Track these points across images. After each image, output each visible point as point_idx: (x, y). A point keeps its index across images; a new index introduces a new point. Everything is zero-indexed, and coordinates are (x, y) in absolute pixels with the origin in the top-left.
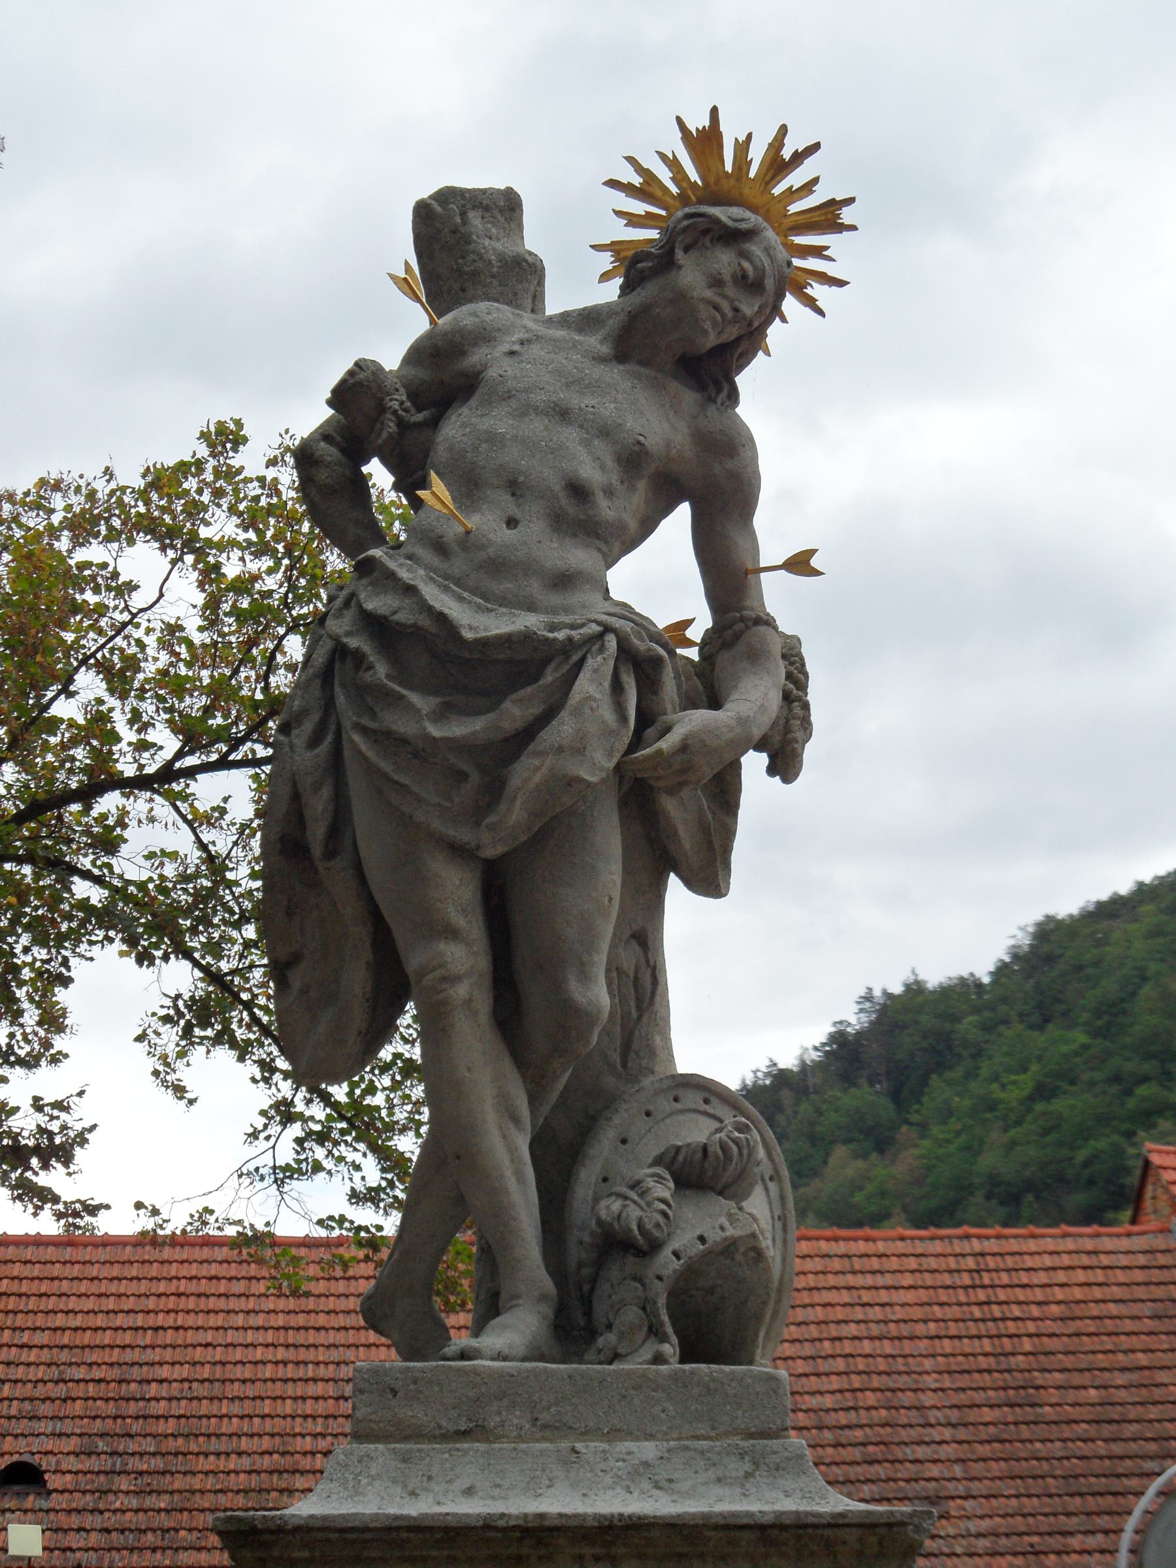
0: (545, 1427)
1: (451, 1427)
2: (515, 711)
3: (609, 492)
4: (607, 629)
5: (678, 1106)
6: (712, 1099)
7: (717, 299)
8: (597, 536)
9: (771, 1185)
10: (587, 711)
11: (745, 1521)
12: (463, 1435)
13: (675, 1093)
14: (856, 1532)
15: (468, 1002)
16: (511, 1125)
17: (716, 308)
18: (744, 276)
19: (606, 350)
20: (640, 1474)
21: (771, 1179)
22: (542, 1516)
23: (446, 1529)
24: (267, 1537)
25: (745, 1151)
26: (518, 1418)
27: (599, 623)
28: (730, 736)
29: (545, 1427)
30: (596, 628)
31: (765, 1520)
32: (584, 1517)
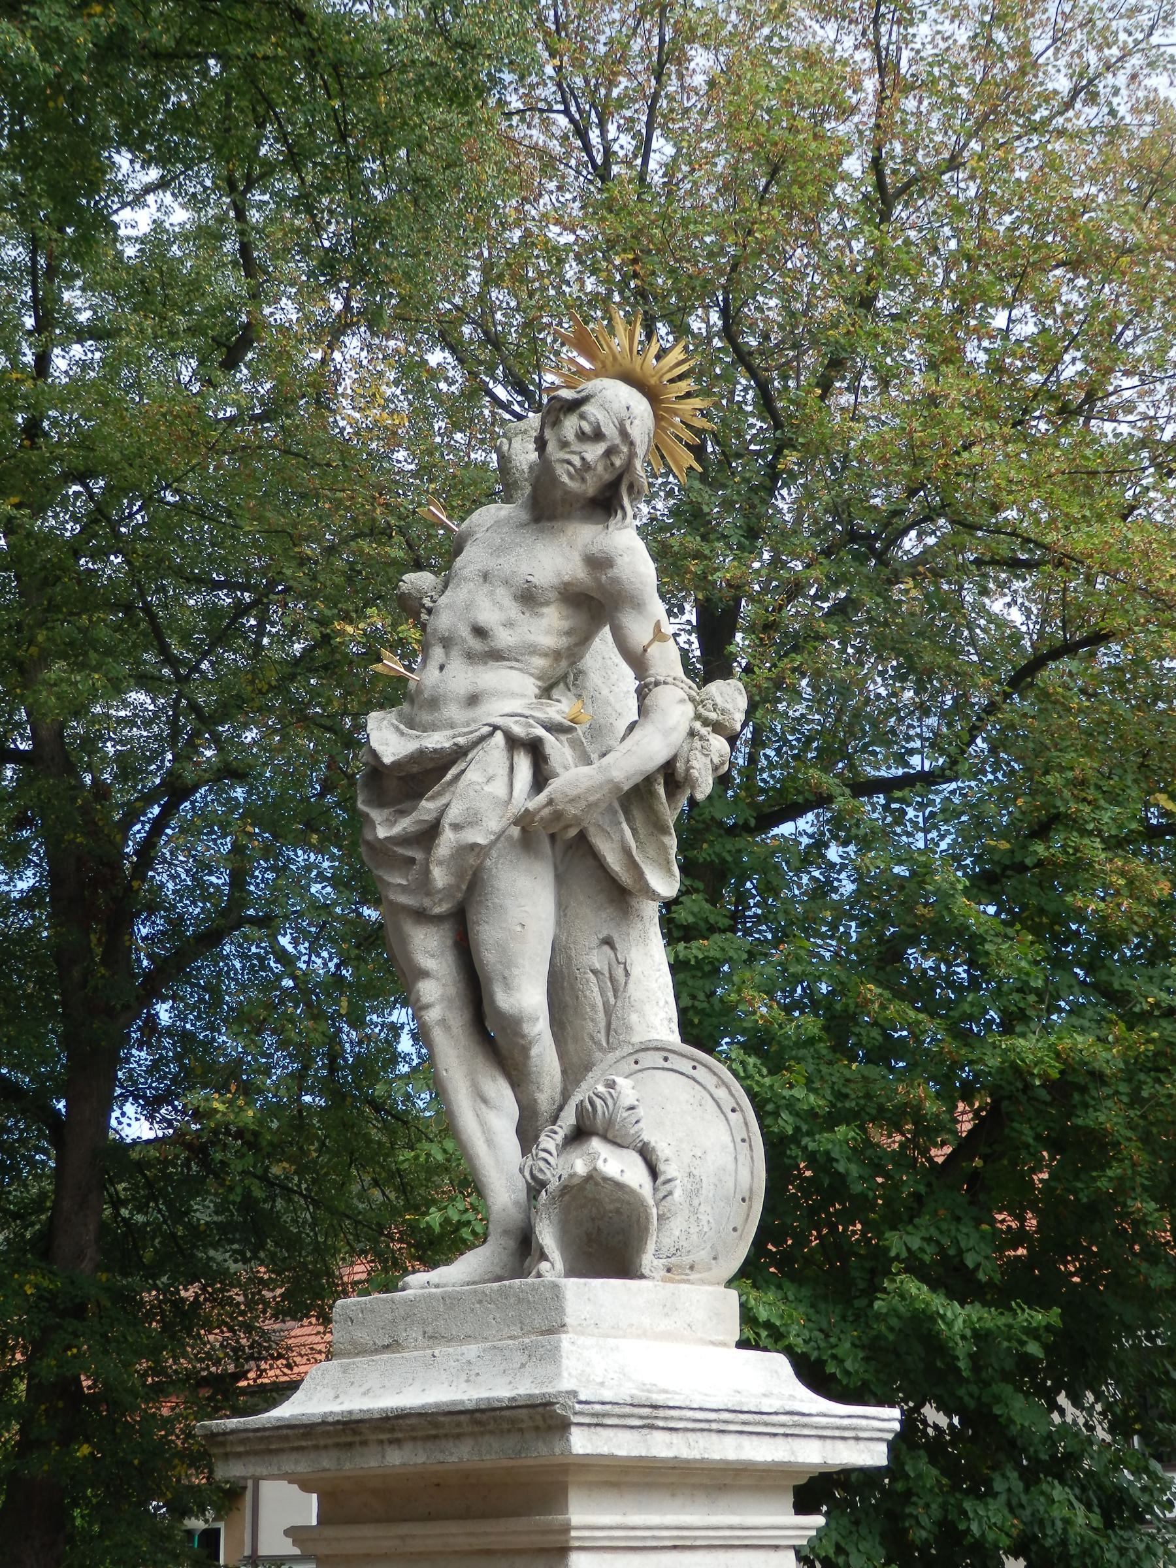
0: (431, 1337)
1: (379, 1343)
2: (428, 807)
3: (509, 624)
4: (496, 728)
5: (638, 1067)
6: (670, 1056)
7: (567, 456)
8: (504, 659)
9: (731, 1116)
10: (472, 793)
11: (460, 1408)
12: (386, 1347)
13: (635, 1057)
14: (524, 1411)
15: (443, 1021)
16: (483, 1106)
17: (569, 462)
18: (583, 433)
19: (524, 516)
20: (469, 1372)
21: (733, 1110)
22: (350, 1412)
23: (305, 1426)
24: (220, 1439)
25: (610, 1102)
26: (415, 1333)
27: (489, 725)
28: (590, 783)
29: (431, 1337)
30: (487, 729)
31: (470, 1406)
32: (462, 1402)
